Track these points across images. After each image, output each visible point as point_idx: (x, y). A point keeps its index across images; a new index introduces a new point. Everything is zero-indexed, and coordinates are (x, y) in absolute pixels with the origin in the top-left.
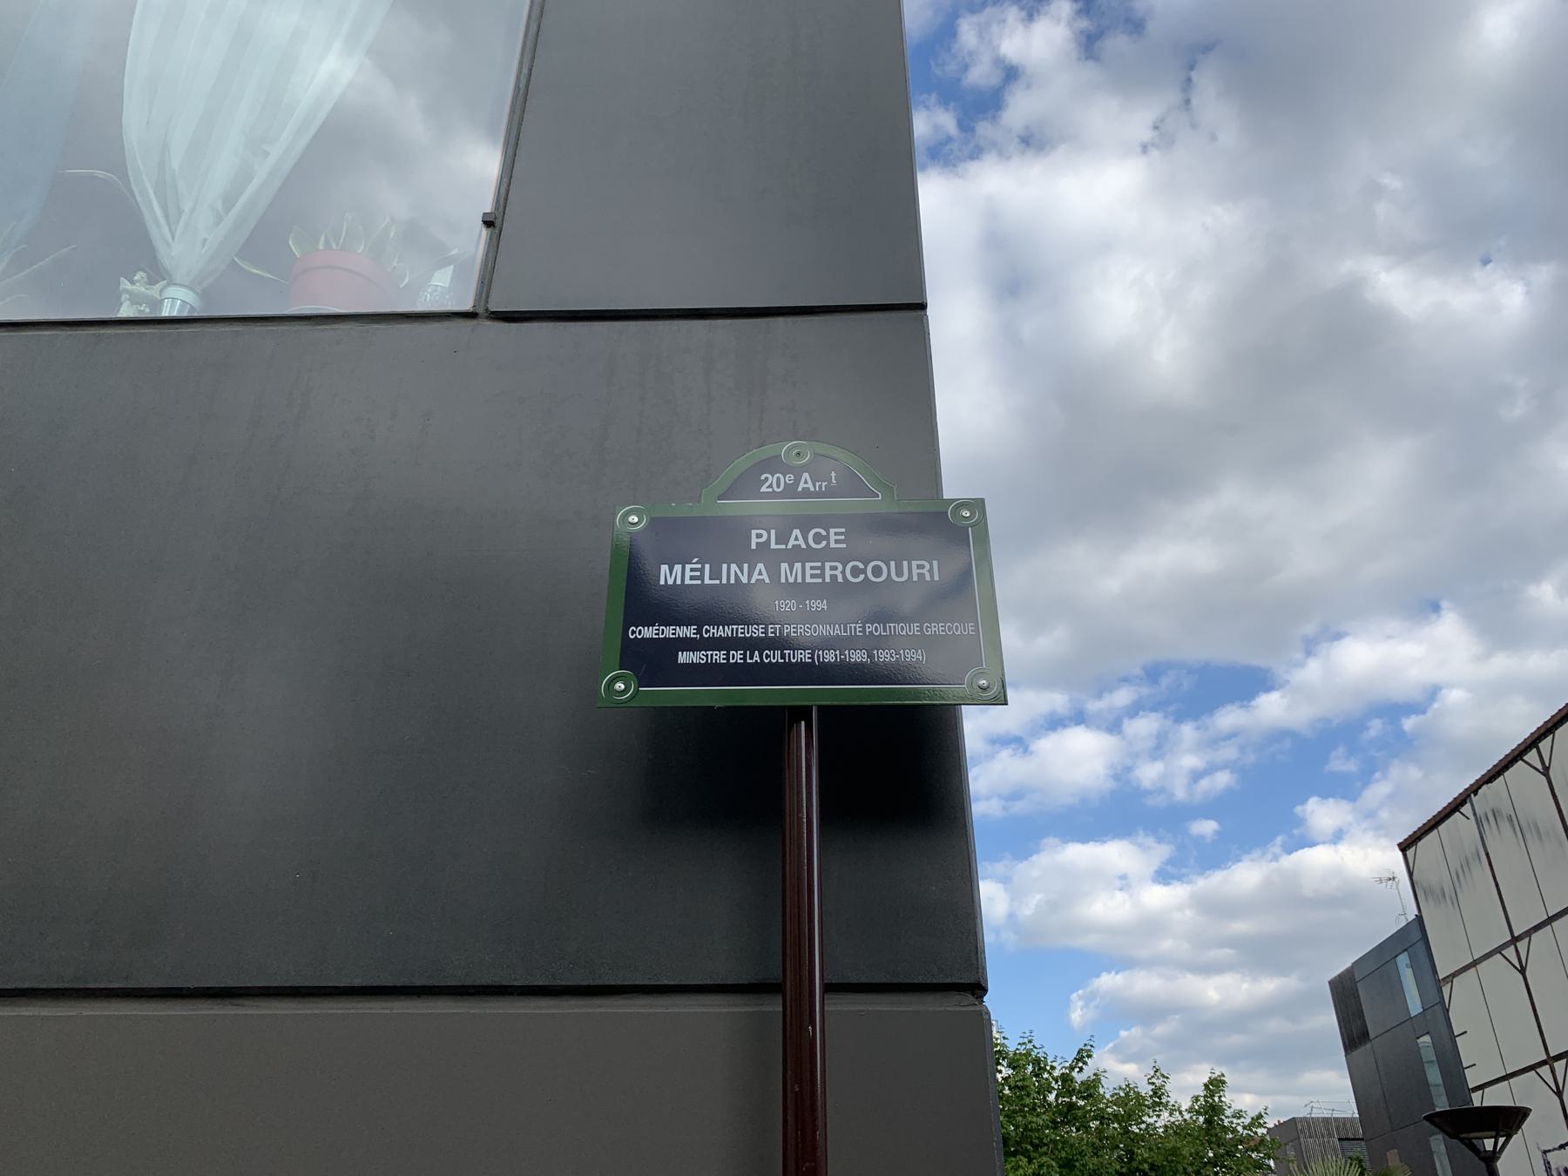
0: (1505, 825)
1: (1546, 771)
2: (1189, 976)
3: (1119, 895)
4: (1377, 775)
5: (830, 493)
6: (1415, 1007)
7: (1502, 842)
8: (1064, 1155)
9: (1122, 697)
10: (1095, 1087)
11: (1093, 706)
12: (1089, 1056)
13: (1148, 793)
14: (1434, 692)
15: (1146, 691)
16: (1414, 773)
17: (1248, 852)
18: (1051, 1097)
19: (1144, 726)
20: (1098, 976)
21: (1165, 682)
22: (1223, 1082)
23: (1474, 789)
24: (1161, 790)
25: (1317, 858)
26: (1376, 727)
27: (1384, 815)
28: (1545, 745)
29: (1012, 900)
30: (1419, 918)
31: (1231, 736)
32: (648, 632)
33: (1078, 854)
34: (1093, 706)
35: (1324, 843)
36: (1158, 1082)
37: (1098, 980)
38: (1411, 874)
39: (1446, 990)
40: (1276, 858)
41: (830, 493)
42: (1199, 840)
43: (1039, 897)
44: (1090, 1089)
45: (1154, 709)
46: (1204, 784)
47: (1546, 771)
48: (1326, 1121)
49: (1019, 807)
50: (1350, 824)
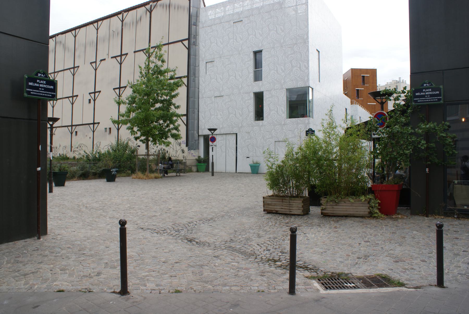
0: (62, 46)
1: (75, 37)
5: (430, 86)
28: (77, 30)
32: (415, 99)
41: (430, 86)
47: (75, 37)
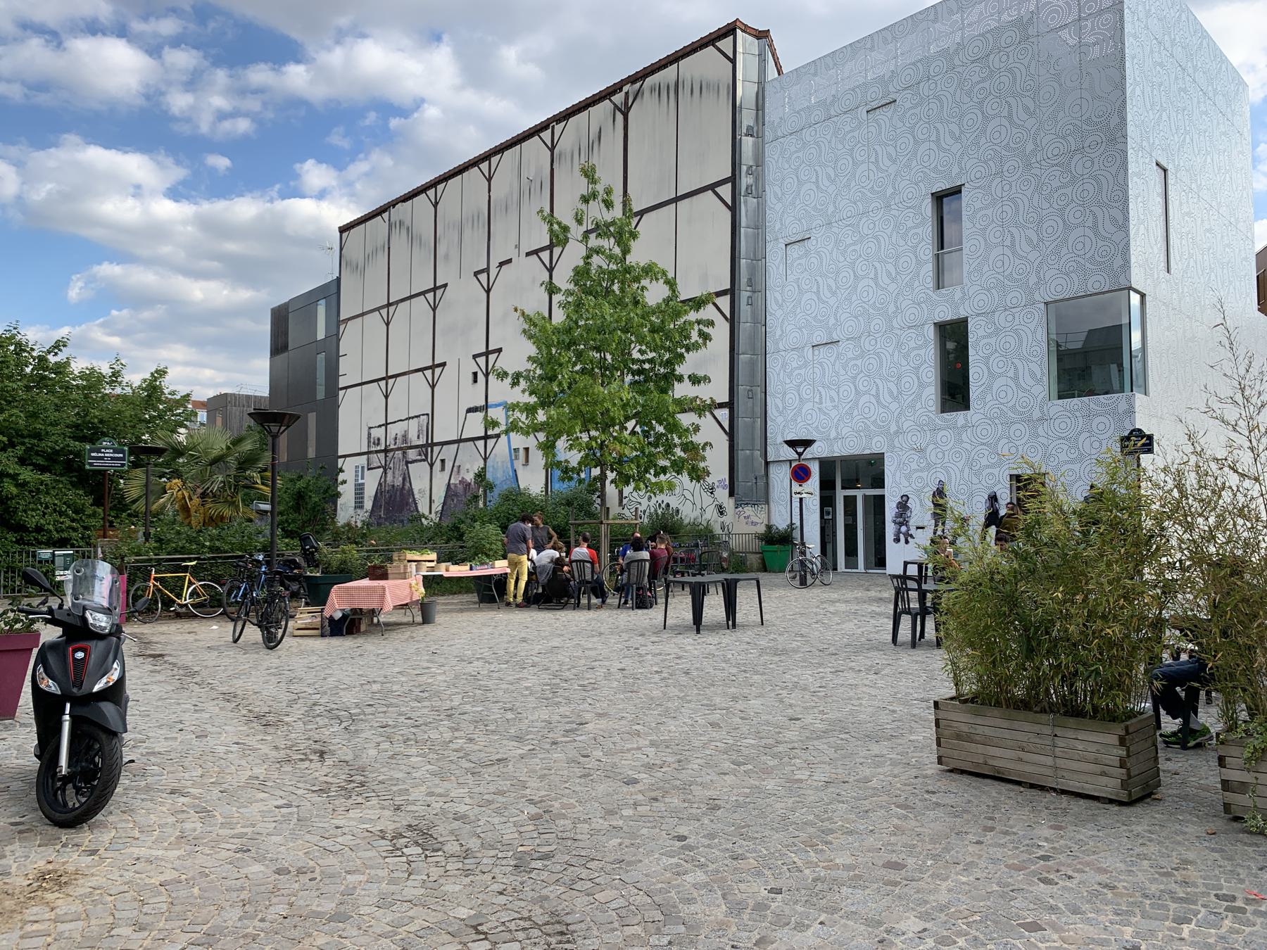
0: (404, 232)
1: (435, 205)
2: (181, 278)
3: (130, 202)
4: (362, 156)
6: (321, 335)
7: (399, 241)
8: (31, 409)
9: (168, 27)
10: (65, 367)
11: (137, 26)
12: (64, 346)
13: (174, 119)
14: (419, 103)
15: (192, 27)
16: (388, 161)
17: (250, 191)
18: (28, 370)
19: (182, 59)
20: (100, 263)
21: (212, 25)
22: (165, 372)
23: (393, 204)
24: (188, 120)
25: (304, 208)
26: (372, 116)
27: (358, 186)
29: (23, 183)
30: (339, 279)
31: (258, 91)
33: (97, 156)
34: (137, 26)
35: (311, 197)
36: (117, 368)
37: (98, 267)
38: (341, 249)
39: (342, 328)
40: (271, 201)
42: (213, 171)
43: (49, 186)
44: (61, 368)
45: (196, 47)
46: (227, 125)
47: (435, 205)
48: (248, 397)
49: (42, 99)
50: (333, 187)
